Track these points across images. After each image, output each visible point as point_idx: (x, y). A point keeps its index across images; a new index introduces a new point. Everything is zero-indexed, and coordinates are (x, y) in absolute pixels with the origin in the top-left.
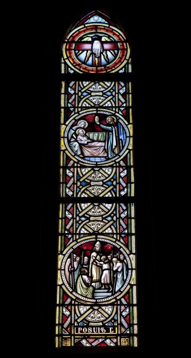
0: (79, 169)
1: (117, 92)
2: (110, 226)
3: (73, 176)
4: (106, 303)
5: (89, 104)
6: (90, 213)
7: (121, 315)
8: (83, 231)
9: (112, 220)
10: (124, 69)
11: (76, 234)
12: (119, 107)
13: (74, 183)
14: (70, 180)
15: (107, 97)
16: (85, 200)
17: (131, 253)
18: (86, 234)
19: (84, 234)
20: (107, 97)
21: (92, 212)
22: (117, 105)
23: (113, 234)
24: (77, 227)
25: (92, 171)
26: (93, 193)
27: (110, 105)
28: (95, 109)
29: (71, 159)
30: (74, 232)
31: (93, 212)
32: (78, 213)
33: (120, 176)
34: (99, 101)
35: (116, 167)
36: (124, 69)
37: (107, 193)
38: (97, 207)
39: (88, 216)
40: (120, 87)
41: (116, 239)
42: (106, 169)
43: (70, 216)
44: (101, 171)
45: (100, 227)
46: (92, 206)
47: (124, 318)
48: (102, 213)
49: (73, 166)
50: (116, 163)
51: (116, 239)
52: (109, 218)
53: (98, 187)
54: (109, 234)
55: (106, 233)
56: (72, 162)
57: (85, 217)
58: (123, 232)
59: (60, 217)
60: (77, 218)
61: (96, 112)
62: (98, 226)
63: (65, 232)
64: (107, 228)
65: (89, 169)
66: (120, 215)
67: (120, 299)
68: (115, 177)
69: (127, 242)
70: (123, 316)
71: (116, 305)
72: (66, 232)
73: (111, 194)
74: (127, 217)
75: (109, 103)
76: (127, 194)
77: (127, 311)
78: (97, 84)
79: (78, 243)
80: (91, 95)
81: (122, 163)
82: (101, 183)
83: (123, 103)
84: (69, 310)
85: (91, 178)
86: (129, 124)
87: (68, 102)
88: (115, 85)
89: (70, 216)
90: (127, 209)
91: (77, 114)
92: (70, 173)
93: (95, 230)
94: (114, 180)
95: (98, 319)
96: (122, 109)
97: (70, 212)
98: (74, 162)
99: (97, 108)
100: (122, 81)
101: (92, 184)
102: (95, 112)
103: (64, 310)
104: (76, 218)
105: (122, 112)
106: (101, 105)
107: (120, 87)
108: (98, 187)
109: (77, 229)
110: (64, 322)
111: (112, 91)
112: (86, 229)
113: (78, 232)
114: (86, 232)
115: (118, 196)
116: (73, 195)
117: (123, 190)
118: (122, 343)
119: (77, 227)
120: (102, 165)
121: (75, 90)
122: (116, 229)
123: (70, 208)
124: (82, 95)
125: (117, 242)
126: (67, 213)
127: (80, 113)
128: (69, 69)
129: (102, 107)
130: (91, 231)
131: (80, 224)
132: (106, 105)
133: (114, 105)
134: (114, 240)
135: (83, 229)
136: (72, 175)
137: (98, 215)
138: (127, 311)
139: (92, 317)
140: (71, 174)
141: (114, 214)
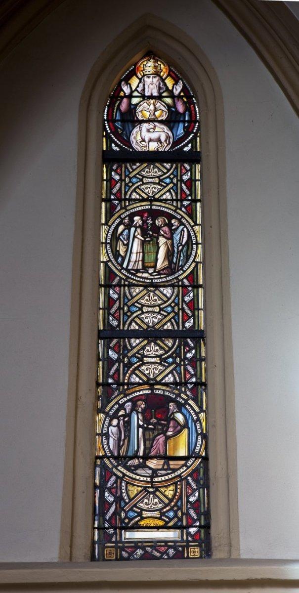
0: (126, 288)
1: (179, 178)
2: (169, 191)
3: (119, 298)
4: (167, 284)
5: (140, 378)
6: (143, 173)
7: (188, 501)
8: (135, 196)
9: (172, 182)
10: (190, 145)
11: (125, 199)
12: (186, 383)
13: (119, 308)
14: (116, 184)
15: (166, 314)
16: (136, 334)
17: (196, 224)
18: (139, 199)
19: (136, 200)
20: (166, 314)
21: (145, 299)
22: (179, 198)
23: (172, 200)
24: (127, 190)
25: (145, 291)
26: (147, 374)
27: (169, 197)
28: (149, 203)
29: (117, 275)
30: (123, 197)
31: (147, 172)
32: (126, 300)
33: (183, 301)
34: (155, 190)
35: (178, 286)
36: (190, 145)
37: (164, 194)
38: (152, 294)
39: (141, 177)
40: (184, 171)
41: (177, 207)
42: (165, 491)
43: (117, 177)
44: (158, 493)
45: (156, 190)
46: (145, 291)
47: (187, 304)
48: (160, 302)
49: (119, 285)
50: (179, 281)
51: (177, 207)
52: (170, 360)
53: (153, 366)
54: (167, 200)
55: (163, 200)
56: (117, 279)
57: (137, 357)
58: (189, 379)
59: (103, 240)
60: (127, 179)
61: (149, 207)
62: (154, 319)
63: (110, 197)
64: (167, 375)
65: (141, 288)
66: (181, 176)
67: (182, 280)
68: (176, 301)
69: (190, 212)
70: (185, 302)
71: (176, 286)
72: (112, 197)
73: (172, 324)
74: (190, 179)
75: (168, 194)
76: (193, 326)
77: (196, 495)
78: (153, 344)
79: (127, 210)
80: (142, 310)
81: (186, 282)
82: (157, 309)
83: (187, 196)
84: (117, 320)
85: (144, 173)
86: (196, 224)
87: (111, 193)
88: (176, 168)
89: (117, 177)
90: (190, 170)
91: (124, 210)
92: (114, 321)
93: (151, 194)
94: (176, 176)
95: (155, 506)
96: (185, 203)
97: (115, 318)
98: (121, 279)
99: (151, 201)
100: (186, 162)
101: (144, 311)
102: (147, 207)
103: (111, 292)
104: (125, 180)
105: (186, 208)
106: (157, 197)
107: (184, 171)
108: (153, 366)
109: (126, 193)
110: (110, 306)
111: (172, 176)
112: (138, 194)
113: (127, 197)
114: (138, 197)
115: (181, 329)
116: (118, 325)
117: (192, 494)
118: (190, 553)
119: (127, 190)
120: (160, 284)
121: (120, 175)
122: (176, 194)
123: (115, 345)
124: (130, 182)
125: (178, 211)
126: (113, 173)
127: (127, 392)
128: (113, 145)
129: (159, 200)
130: (145, 196)
131: (129, 317)
132: (164, 197)
133: (174, 198)
134: (174, 208)
135: (134, 194)
136: (117, 324)
137: (155, 354)
138: (196, 495)
139: (146, 503)
140: (115, 296)
141: (175, 303)
